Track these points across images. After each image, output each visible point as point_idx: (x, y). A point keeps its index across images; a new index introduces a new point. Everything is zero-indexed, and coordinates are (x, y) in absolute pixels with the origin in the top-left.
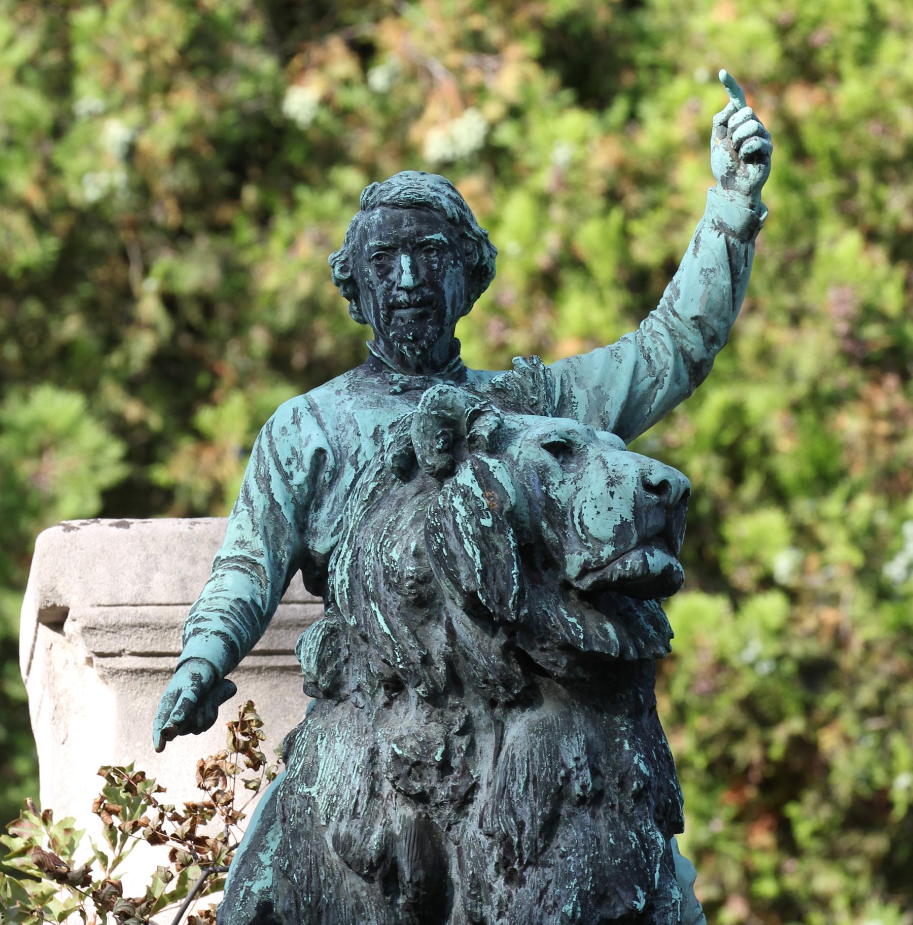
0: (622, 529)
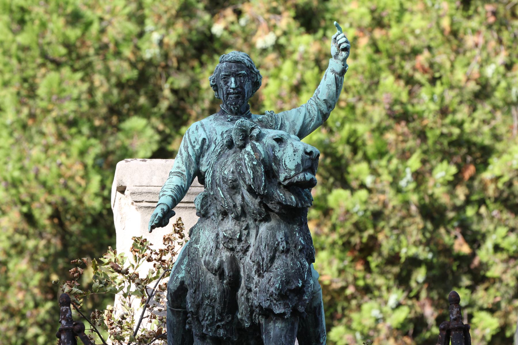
0: (297, 166)
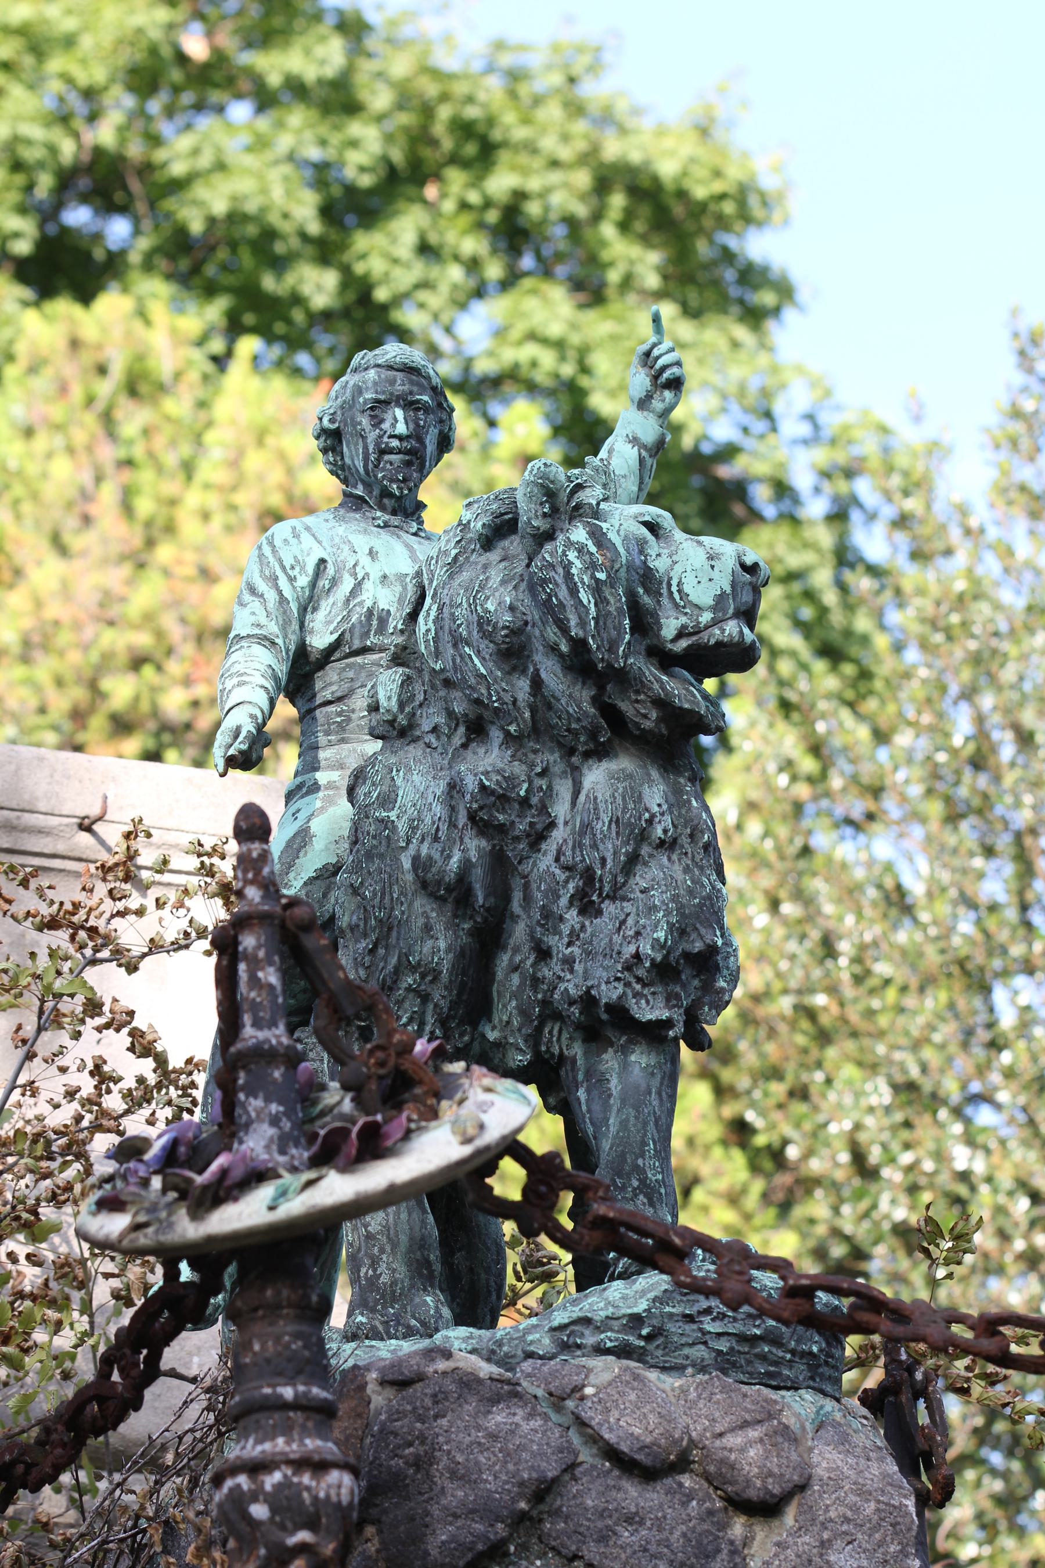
0: (721, 599)
